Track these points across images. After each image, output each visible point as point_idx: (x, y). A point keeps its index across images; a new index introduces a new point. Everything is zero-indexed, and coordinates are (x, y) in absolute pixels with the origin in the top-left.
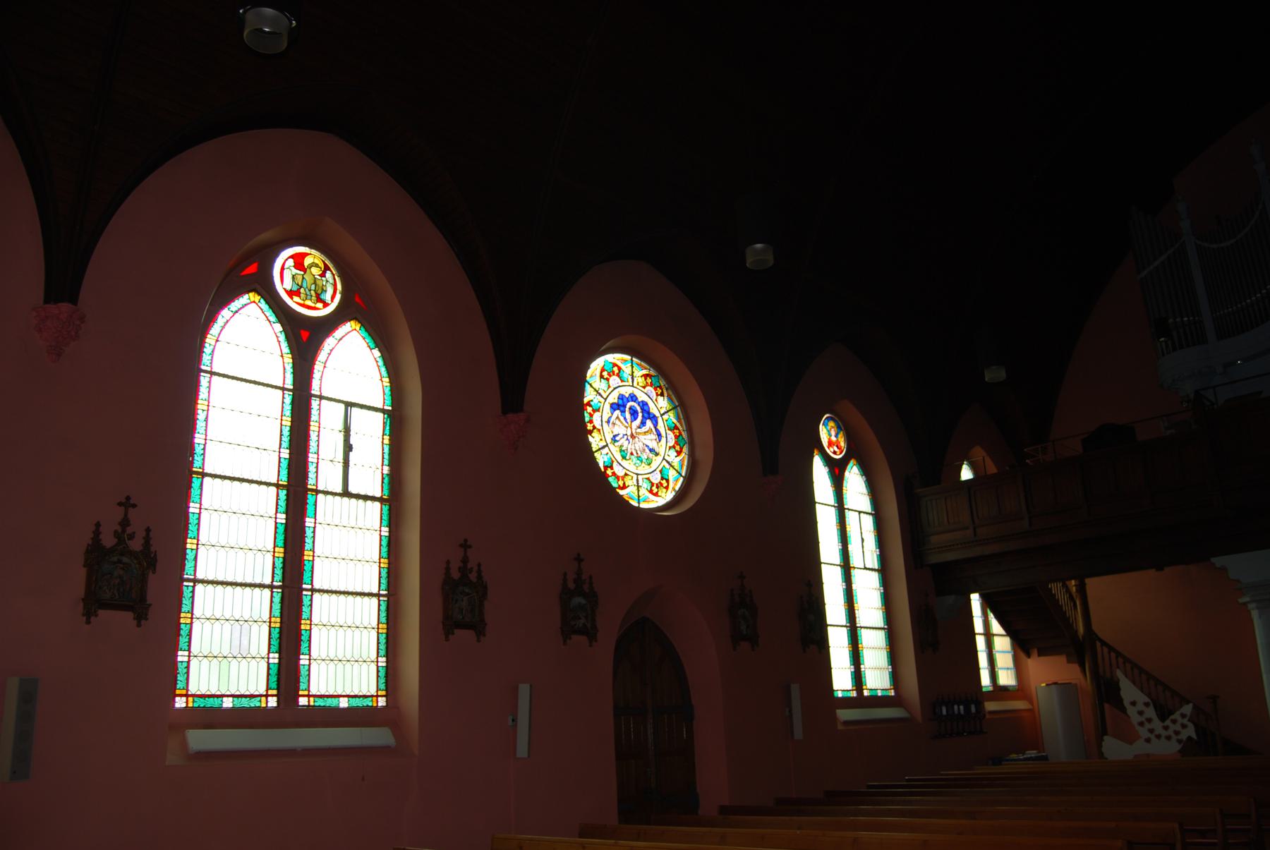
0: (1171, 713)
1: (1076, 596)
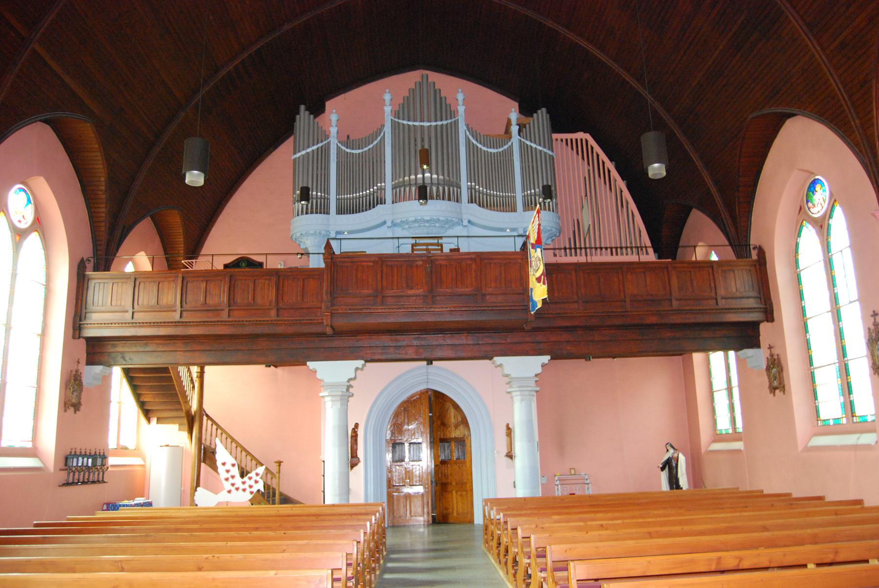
0: (248, 473)
1: (196, 381)
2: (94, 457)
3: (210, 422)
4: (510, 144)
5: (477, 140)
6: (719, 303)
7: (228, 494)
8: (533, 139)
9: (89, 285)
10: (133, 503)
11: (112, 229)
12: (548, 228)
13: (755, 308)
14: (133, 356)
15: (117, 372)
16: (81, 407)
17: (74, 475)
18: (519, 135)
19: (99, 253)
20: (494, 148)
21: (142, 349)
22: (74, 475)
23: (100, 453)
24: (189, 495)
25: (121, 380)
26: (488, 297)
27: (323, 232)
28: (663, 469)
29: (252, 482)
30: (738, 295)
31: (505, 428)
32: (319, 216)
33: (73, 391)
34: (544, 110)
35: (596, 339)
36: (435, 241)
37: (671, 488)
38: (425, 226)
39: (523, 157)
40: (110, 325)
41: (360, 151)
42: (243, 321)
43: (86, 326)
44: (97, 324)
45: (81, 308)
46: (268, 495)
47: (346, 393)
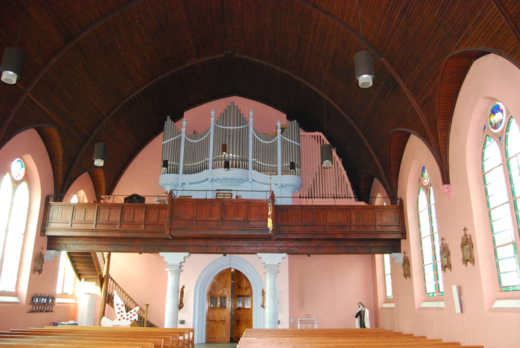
0: (131, 309)
2: (48, 298)
3: (112, 282)
4: (276, 139)
5: (259, 137)
6: (377, 229)
7: (119, 321)
8: (286, 136)
9: (51, 209)
10: (67, 323)
11: (65, 180)
12: (294, 184)
13: (396, 232)
14: (71, 246)
15: (64, 255)
16: (42, 272)
17: (36, 307)
18: (281, 134)
19: (58, 192)
20: (267, 141)
21: (76, 243)
22: (36, 307)
23: (51, 296)
24: (99, 321)
25: (66, 259)
26: (251, 222)
27: (175, 184)
28: (356, 317)
29: (132, 315)
30: (388, 224)
31: (261, 291)
32: (173, 175)
33: (39, 263)
34: (295, 121)
35: (311, 246)
36: (229, 192)
37: (361, 327)
38: (229, 181)
39: (283, 146)
40: (60, 230)
41: (197, 141)
42: (127, 230)
43: (47, 230)
44: (53, 229)
45: (46, 220)
46: (141, 322)
47: (179, 269)
